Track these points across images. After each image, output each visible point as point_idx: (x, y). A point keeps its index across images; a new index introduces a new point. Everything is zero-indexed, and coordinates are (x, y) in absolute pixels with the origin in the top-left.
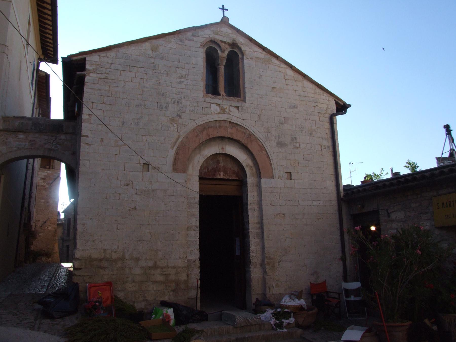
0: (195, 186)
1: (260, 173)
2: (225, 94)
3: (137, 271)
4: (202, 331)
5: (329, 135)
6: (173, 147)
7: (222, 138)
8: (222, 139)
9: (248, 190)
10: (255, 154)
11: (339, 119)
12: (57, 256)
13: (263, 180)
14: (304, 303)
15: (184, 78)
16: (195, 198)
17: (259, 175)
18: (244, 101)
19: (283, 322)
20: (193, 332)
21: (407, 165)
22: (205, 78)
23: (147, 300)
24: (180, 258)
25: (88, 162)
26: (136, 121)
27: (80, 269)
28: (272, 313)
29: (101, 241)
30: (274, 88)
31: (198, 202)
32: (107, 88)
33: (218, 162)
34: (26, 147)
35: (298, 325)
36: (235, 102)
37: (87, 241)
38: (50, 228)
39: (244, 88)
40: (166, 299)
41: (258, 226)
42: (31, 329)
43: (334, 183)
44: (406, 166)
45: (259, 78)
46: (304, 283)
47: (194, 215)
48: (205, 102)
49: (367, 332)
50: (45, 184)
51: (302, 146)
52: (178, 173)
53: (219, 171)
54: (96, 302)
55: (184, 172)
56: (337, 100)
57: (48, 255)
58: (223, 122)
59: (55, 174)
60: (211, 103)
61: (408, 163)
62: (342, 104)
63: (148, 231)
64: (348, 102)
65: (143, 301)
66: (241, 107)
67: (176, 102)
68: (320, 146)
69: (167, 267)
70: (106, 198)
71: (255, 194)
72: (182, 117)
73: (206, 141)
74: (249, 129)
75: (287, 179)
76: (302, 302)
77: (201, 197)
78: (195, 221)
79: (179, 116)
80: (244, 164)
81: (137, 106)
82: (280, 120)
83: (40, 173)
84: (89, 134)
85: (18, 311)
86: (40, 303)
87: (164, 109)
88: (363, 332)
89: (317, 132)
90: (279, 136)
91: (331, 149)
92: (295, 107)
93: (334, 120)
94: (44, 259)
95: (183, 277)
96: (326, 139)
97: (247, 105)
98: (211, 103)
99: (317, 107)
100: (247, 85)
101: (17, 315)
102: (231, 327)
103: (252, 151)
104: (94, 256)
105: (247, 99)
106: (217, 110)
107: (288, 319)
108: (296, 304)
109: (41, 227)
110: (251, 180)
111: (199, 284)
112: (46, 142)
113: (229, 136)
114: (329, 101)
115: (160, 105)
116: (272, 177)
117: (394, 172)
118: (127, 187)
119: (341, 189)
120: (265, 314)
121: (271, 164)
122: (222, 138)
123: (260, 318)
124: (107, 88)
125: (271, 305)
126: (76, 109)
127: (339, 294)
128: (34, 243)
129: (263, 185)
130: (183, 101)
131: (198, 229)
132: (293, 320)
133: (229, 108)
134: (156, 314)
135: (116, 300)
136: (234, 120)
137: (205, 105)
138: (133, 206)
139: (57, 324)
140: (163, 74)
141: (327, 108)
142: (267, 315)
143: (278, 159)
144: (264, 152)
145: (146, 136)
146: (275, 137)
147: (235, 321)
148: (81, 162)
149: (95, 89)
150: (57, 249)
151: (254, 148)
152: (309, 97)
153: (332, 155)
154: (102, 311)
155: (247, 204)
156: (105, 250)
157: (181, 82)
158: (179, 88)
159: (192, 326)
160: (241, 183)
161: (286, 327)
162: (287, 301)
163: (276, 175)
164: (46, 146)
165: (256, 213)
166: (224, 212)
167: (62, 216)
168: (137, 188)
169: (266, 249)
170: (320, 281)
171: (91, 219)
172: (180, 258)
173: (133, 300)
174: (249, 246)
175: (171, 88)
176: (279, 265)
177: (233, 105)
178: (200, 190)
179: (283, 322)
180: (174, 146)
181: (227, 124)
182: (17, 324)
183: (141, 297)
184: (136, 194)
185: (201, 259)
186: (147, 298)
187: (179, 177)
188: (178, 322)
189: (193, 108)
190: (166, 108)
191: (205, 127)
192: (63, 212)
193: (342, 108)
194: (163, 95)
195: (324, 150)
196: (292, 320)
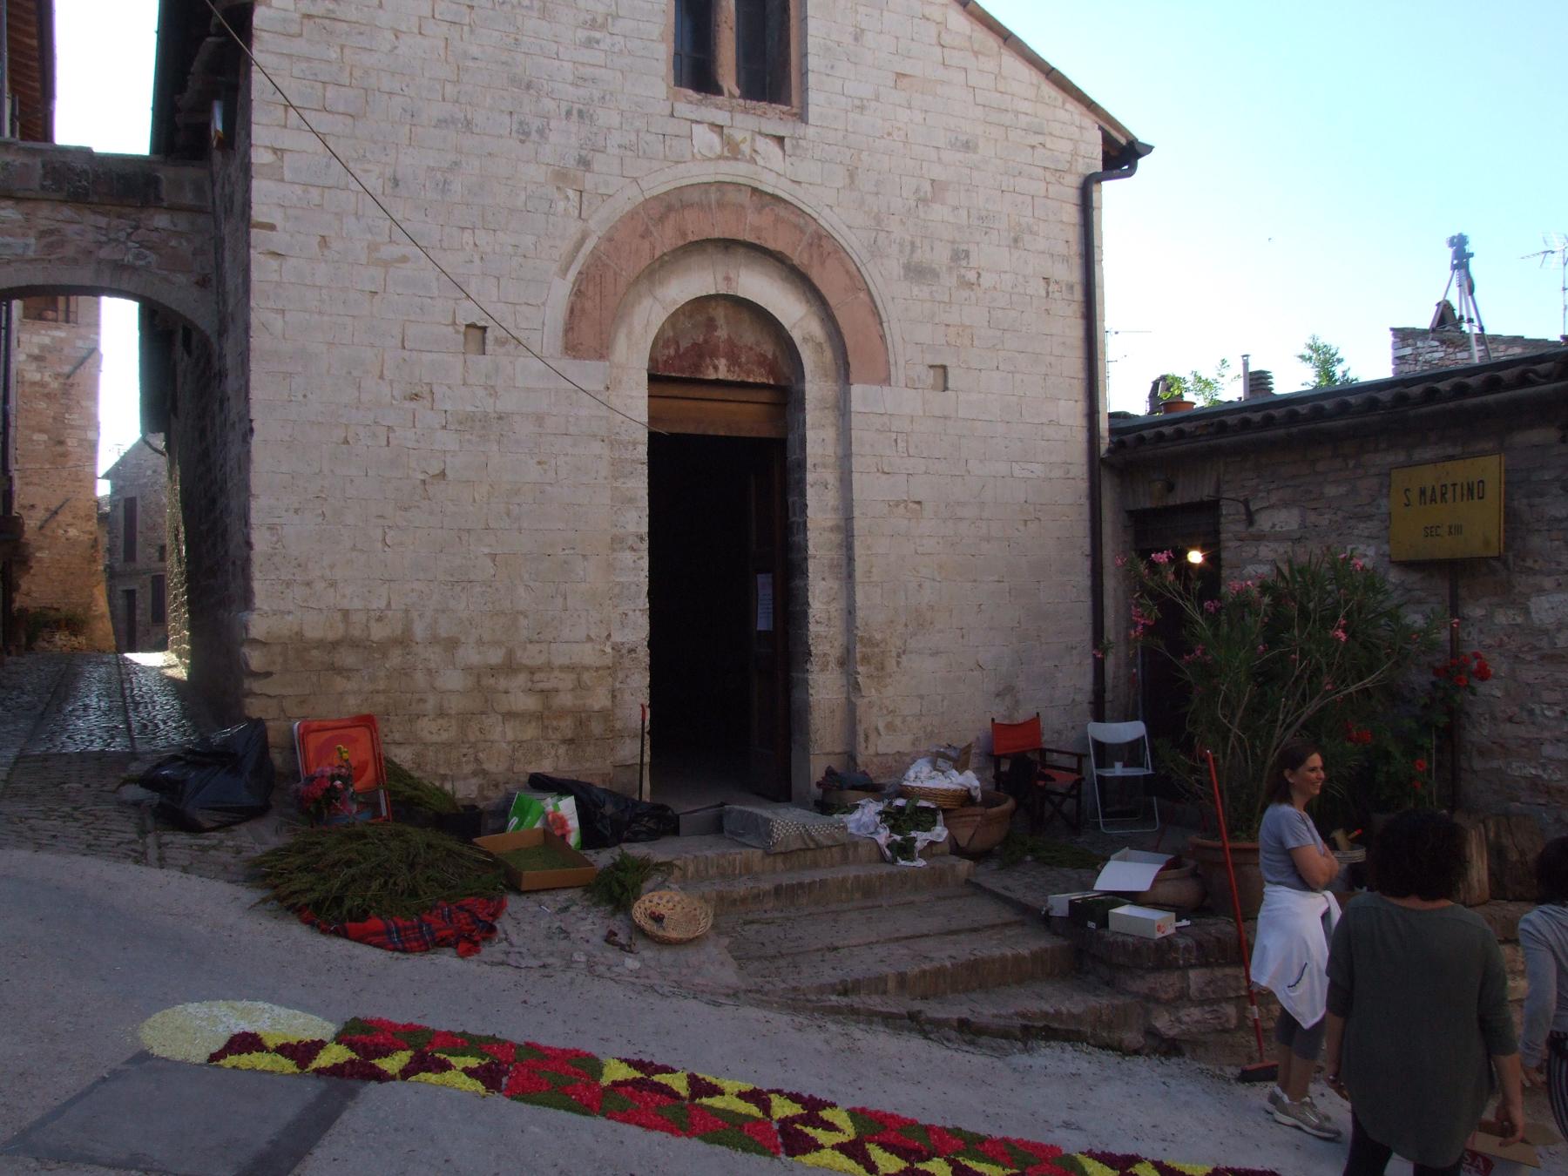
0: (635, 402)
1: (847, 364)
2: (737, 92)
3: (453, 680)
4: (670, 865)
5: (1075, 248)
6: (564, 271)
7: (728, 245)
8: (727, 248)
9: (808, 418)
10: (832, 301)
11: (1111, 193)
12: (104, 628)
13: (857, 390)
14: (977, 783)
15: (603, 26)
16: (635, 444)
17: (843, 371)
18: (802, 117)
19: (914, 840)
20: (644, 868)
21: (1308, 353)
22: (672, 29)
23: (485, 773)
24: (589, 639)
25: (279, 317)
26: (439, 175)
27: (268, 674)
28: (880, 813)
29: (333, 584)
30: (904, 75)
31: (645, 458)
32: (333, 54)
33: (711, 324)
34: (31, 254)
35: (957, 850)
36: (771, 119)
37: (288, 584)
38: (72, 532)
39: (804, 74)
40: (546, 767)
41: (836, 538)
42: (137, 862)
43: (1080, 407)
44: (1302, 357)
45: (856, 39)
46: (973, 719)
47: (631, 500)
48: (672, 115)
49: (1168, 866)
50: (47, 379)
51: (988, 280)
52: (582, 358)
53: (714, 354)
54: (333, 778)
55: (602, 357)
56: (1107, 127)
57: (74, 624)
58: (731, 188)
59: (80, 343)
60: (694, 121)
61: (1311, 347)
62: (1123, 141)
63: (486, 550)
64: (1143, 137)
65: (475, 774)
66: (792, 137)
67: (575, 112)
68: (1042, 283)
69: (549, 667)
70: (346, 442)
71: (830, 434)
72: (595, 167)
73: (674, 251)
74: (815, 215)
75: (934, 388)
76: (968, 780)
77: (653, 437)
78: (637, 521)
79: (585, 163)
80: (796, 335)
81: (442, 123)
82: (917, 190)
83: (24, 337)
84: (276, 217)
85: (75, 809)
86: (147, 782)
87: (534, 136)
88: (1156, 868)
89: (1037, 234)
90: (913, 244)
91: (1078, 294)
92: (968, 146)
93: (1095, 196)
94: (61, 638)
95: (599, 700)
96: (1065, 259)
97: (811, 131)
98: (694, 121)
99: (1040, 150)
100: (813, 62)
101: (77, 820)
102: (759, 852)
103: (824, 291)
104: (312, 633)
105: (813, 111)
106: (711, 148)
107: (928, 830)
108: (953, 787)
109: (41, 528)
110: (816, 388)
111: (647, 723)
112: (104, 239)
113: (750, 237)
114: (1081, 128)
115: (521, 123)
116: (887, 380)
117: (1252, 369)
118: (413, 405)
119: (1104, 425)
120: (857, 815)
121: (882, 337)
122: (728, 245)
123: (845, 828)
124: (333, 54)
125: (873, 789)
126: (218, 125)
127: (1081, 757)
128: (25, 584)
129: (856, 406)
130: (599, 111)
131: (646, 545)
132: (945, 833)
133: (753, 140)
134: (523, 814)
135: (390, 772)
136: (769, 184)
137: (672, 127)
138: (435, 468)
139: (214, 847)
140: (530, 8)
141: (1075, 154)
142: (865, 816)
143: (910, 320)
144: (862, 295)
145: (473, 229)
146: (901, 245)
147: (771, 837)
148: (255, 319)
149: (290, 56)
150: (102, 605)
151: (828, 280)
152: (1017, 113)
153: (1079, 314)
154: (355, 808)
155: (802, 465)
156: (346, 614)
157: (590, 43)
158: (583, 64)
159: (638, 850)
160: (785, 397)
161: (922, 854)
162: (922, 776)
163: (898, 374)
164: (104, 253)
165: (831, 497)
166: (726, 496)
167: (104, 489)
168: (448, 407)
169: (860, 614)
170: (1021, 716)
171: (296, 511)
172: (589, 639)
173: (442, 772)
174: (808, 604)
175: (557, 63)
176: (898, 663)
177: (764, 130)
178: (652, 419)
179: (914, 840)
180: (567, 269)
181: (745, 198)
182: (89, 846)
183: (467, 763)
184: (444, 427)
185: (656, 642)
186: (485, 766)
187: (588, 373)
188: (593, 836)
189: (633, 137)
190: (541, 132)
191: (670, 205)
192: (106, 476)
193: (1122, 154)
194: (529, 86)
195: (1057, 295)
196: (940, 833)
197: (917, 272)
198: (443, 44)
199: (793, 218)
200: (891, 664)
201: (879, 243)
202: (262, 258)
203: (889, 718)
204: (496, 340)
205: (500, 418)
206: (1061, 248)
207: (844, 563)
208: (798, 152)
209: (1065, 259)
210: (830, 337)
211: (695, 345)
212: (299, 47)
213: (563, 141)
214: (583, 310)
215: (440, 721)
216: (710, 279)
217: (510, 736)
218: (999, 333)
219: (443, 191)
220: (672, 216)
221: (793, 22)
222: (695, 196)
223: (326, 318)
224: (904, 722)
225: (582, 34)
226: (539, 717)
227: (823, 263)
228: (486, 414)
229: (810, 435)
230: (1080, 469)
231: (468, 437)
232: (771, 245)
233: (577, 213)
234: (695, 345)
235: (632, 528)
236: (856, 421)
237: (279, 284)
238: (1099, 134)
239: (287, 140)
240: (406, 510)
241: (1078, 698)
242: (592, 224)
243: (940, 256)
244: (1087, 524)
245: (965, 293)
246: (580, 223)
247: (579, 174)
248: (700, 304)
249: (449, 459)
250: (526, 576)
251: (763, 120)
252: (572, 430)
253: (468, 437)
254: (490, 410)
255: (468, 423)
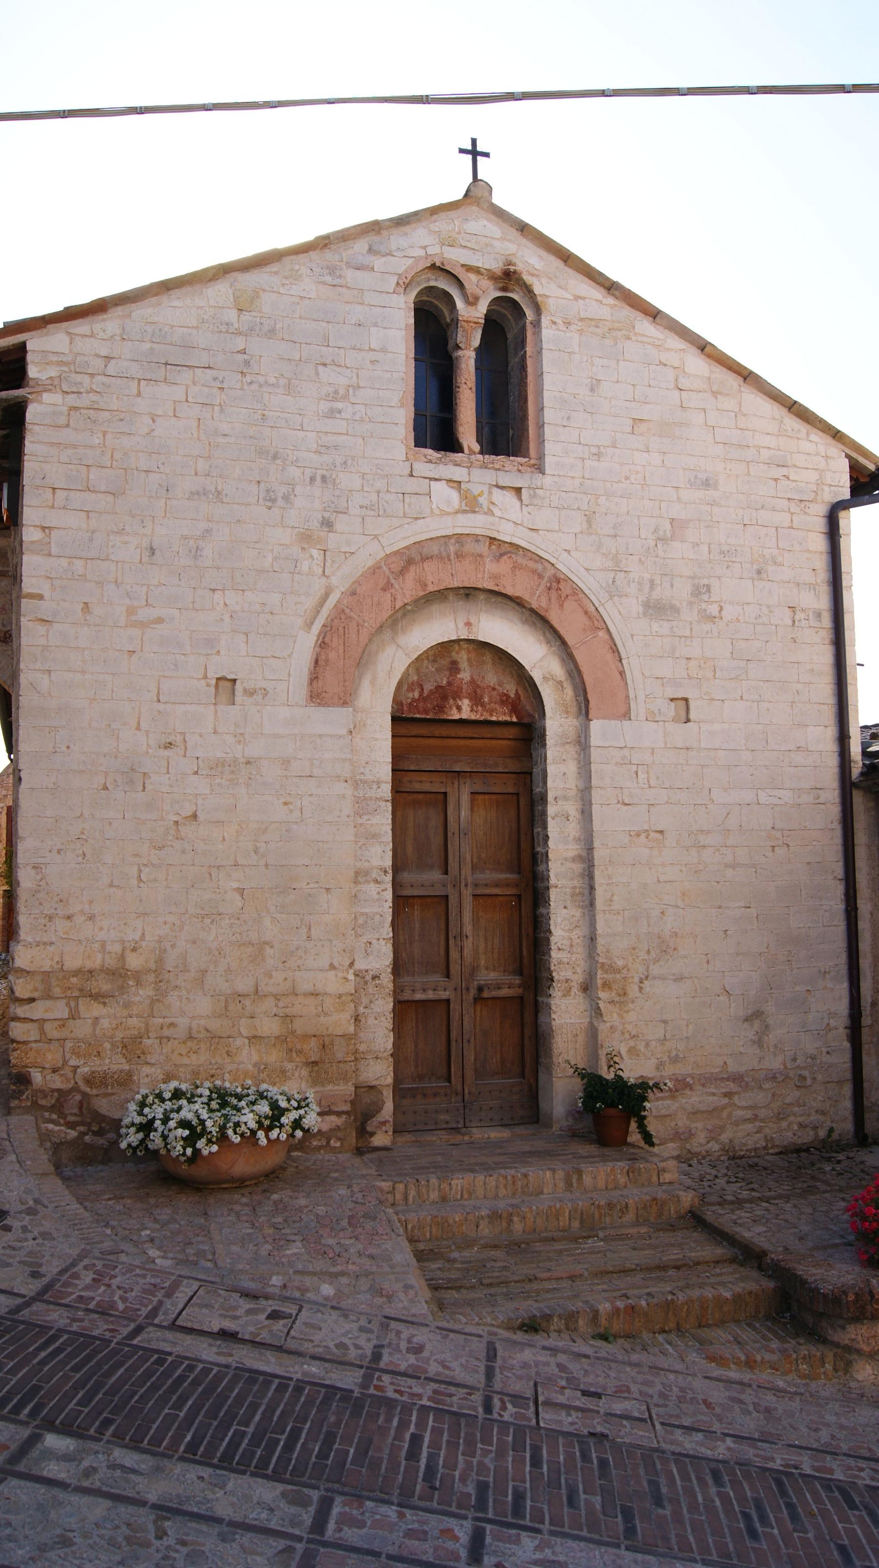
1: (587, 701)
2: (476, 447)
5: (823, 575)
6: (309, 625)
7: (468, 593)
13: (596, 726)
15: (346, 397)
17: (584, 709)
18: (540, 469)
24: (332, 967)
25: (46, 677)
27: (32, 1000)
29: (91, 918)
31: (388, 795)
33: (454, 668)
36: (510, 470)
39: (541, 426)
41: (578, 867)
43: (831, 732)
45: (592, 390)
47: (375, 836)
48: (411, 475)
51: (729, 612)
53: (457, 696)
55: (345, 703)
56: (854, 455)
60: (431, 479)
63: (235, 885)
67: (318, 478)
68: (788, 612)
70: (106, 788)
71: (572, 768)
72: (338, 527)
73: (416, 601)
79: (328, 524)
80: (537, 676)
81: (194, 495)
82: (656, 530)
84: (45, 589)
87: (280, 502)
91: (827, 621)
92: (707, 484)
93: (842, 523)
97: (547, 480)
100: (549, 415)
103: (562, 632)
110: (557, 724)
114: (827, 457)
115: (268, 491)
116: (627, 715)
118: (167, 753)
121: (622, 673)
122: (468, 593)
124: (97, 440)
129: (594, 741)
133: (490, 493)
136: (506, 533)
137: (412, 485)
138: (188, 811)
141: (820, 483)
144: (602, 634)
146: (640, 583)
151: (568, 621)
152: (758, 448)
153: (827, 641)
155: (544, 799)
157: (332, 414)
163: (638, 708)
165: (573, 829)
169: (600, 941)
172: (332, 967)
176: (641, 989)
177: (501, 483)
180: (312, 623)
181: (483, 548)
184: (196, 773)
189: (374, 497)
190: (286, 498)
191: (411, 558)
194: (275, 457)
195: (804, 623)
197: (656, 609)
198: (196, 424)
199: (531, 564)
200: (633, 990)
201: (618, 583)
202: (31, 624)
203: (632, 1043)
204: (245, 691)
205: (248, 763)
206: (807, 577)
207: (586, 892)
208: (535, 501)
209: (812, 587)
210: (570, 674)
211: (438, 687)
212: (66, 435)
213: (308, 504)
214: (327, 661)
215: (189, 1044)
216: (452, 625)
217: (255, 1057)
218: (743, 664)
219: (195, 557)
220: (412, 568)
221: (530, 379)
222: (435, 549)
223: (87, 676)
224: (647, 1045)
225: (324, 406)
226: (281, 1040)
227: (561, 606)
228: (235, 760)
229: (551, 769)
230: (832, 794)
231: (218, 781)
232: (509, 591)
233: (321, 570)
234: (438, 687)
235: (376, 862)
236: (595, 754)
237: (45, 647)
238: (846, 462)
239: (54, 519)
240: (160, 849)
241: (833, 1023)
242: (334, 580)
243: (682, 591)
244: (840, 848)
245: (707, 627)
246: (324, 580)
247: (322, 534)
248: (445, 648)
249: (200, 802)
250: (273, 909)
251: (500, 473)
252: (316, 772)
253: (218, 781)
254: (239, 756)
255: (218, 766)
